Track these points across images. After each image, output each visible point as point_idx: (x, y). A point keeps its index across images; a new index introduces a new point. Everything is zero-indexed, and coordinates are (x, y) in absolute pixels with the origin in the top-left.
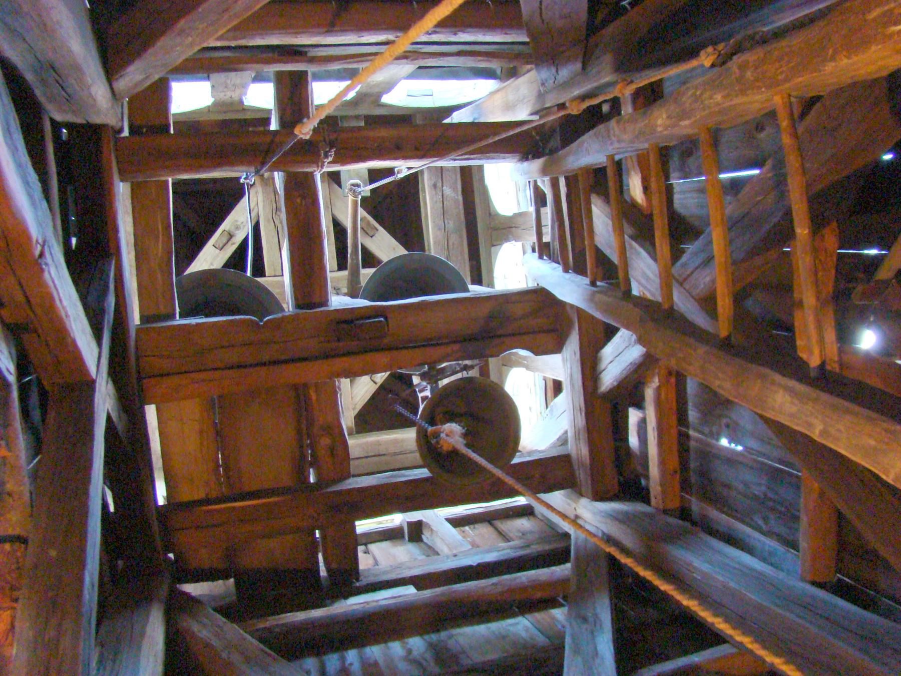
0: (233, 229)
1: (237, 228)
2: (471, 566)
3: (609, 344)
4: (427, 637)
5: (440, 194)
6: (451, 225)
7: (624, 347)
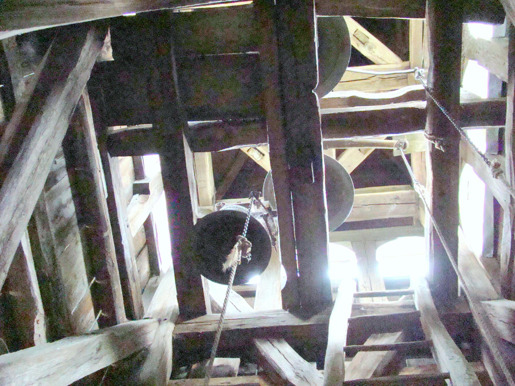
0: (369, 44)
1: (370, 48)
2: (121, 239)
3: (293, 351)
4: (75, 217)
5: (391, 202)
6: (367, 209)
7: (292, 363)
